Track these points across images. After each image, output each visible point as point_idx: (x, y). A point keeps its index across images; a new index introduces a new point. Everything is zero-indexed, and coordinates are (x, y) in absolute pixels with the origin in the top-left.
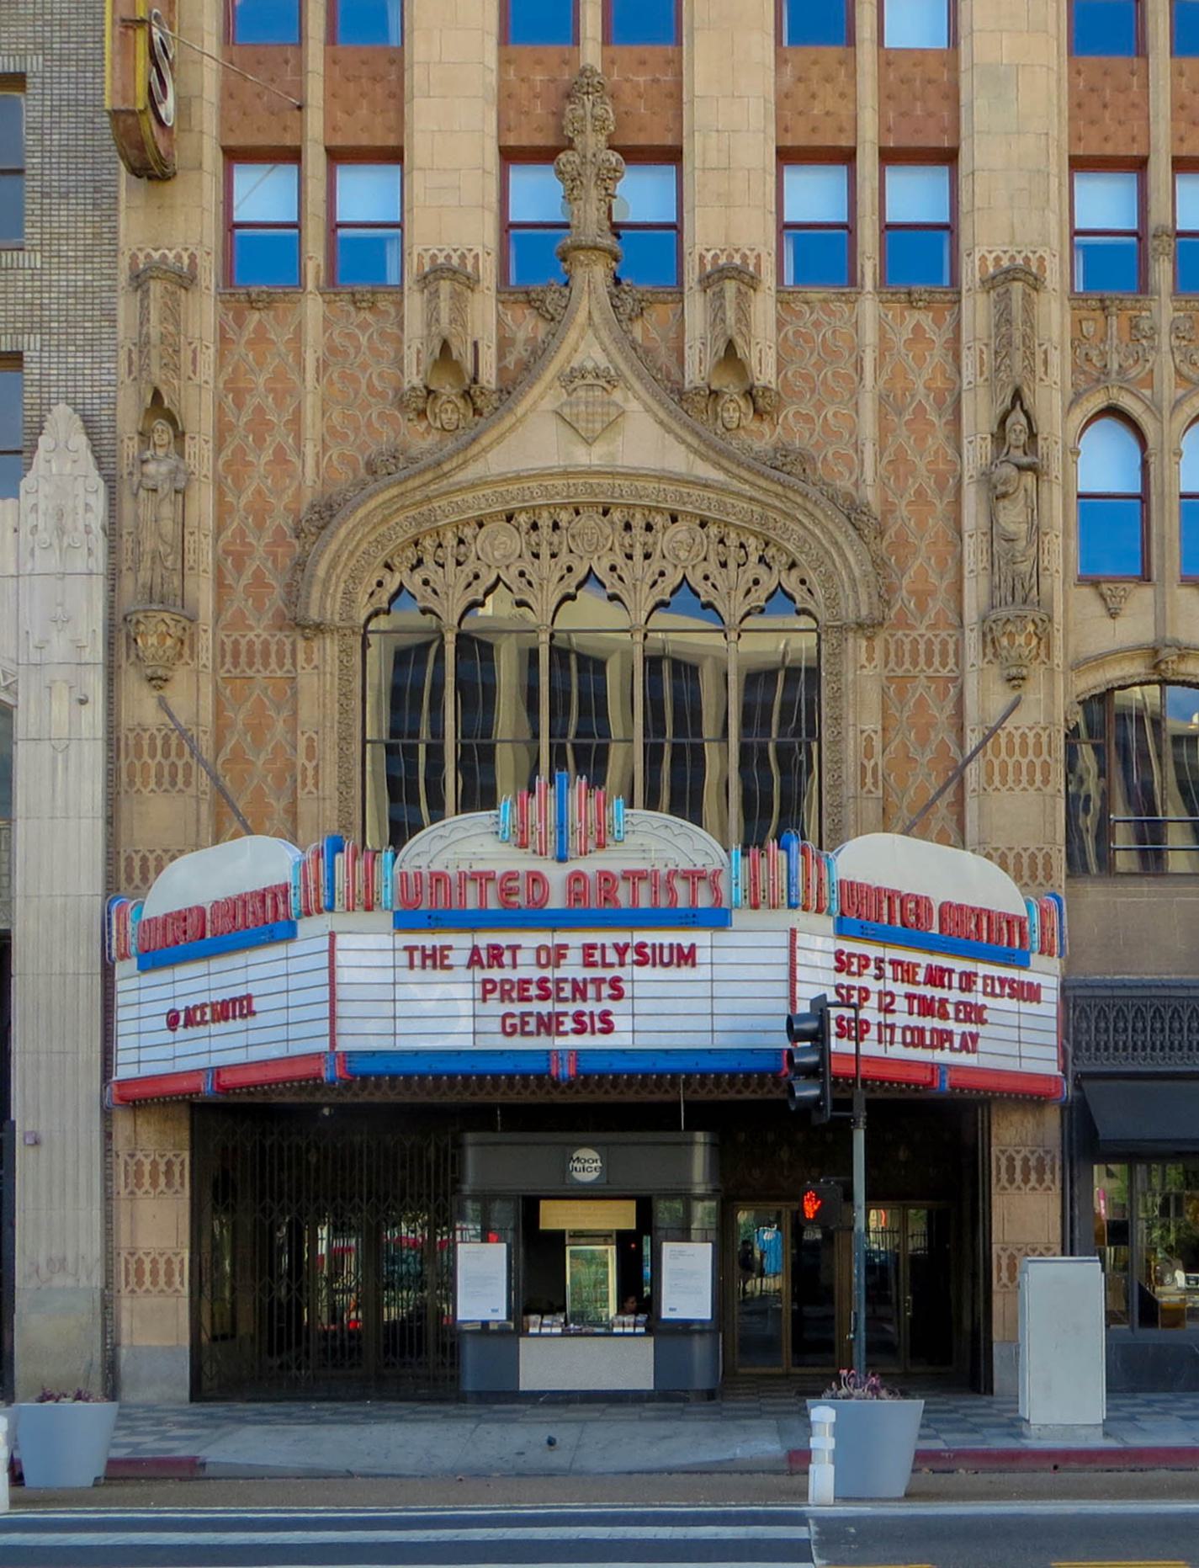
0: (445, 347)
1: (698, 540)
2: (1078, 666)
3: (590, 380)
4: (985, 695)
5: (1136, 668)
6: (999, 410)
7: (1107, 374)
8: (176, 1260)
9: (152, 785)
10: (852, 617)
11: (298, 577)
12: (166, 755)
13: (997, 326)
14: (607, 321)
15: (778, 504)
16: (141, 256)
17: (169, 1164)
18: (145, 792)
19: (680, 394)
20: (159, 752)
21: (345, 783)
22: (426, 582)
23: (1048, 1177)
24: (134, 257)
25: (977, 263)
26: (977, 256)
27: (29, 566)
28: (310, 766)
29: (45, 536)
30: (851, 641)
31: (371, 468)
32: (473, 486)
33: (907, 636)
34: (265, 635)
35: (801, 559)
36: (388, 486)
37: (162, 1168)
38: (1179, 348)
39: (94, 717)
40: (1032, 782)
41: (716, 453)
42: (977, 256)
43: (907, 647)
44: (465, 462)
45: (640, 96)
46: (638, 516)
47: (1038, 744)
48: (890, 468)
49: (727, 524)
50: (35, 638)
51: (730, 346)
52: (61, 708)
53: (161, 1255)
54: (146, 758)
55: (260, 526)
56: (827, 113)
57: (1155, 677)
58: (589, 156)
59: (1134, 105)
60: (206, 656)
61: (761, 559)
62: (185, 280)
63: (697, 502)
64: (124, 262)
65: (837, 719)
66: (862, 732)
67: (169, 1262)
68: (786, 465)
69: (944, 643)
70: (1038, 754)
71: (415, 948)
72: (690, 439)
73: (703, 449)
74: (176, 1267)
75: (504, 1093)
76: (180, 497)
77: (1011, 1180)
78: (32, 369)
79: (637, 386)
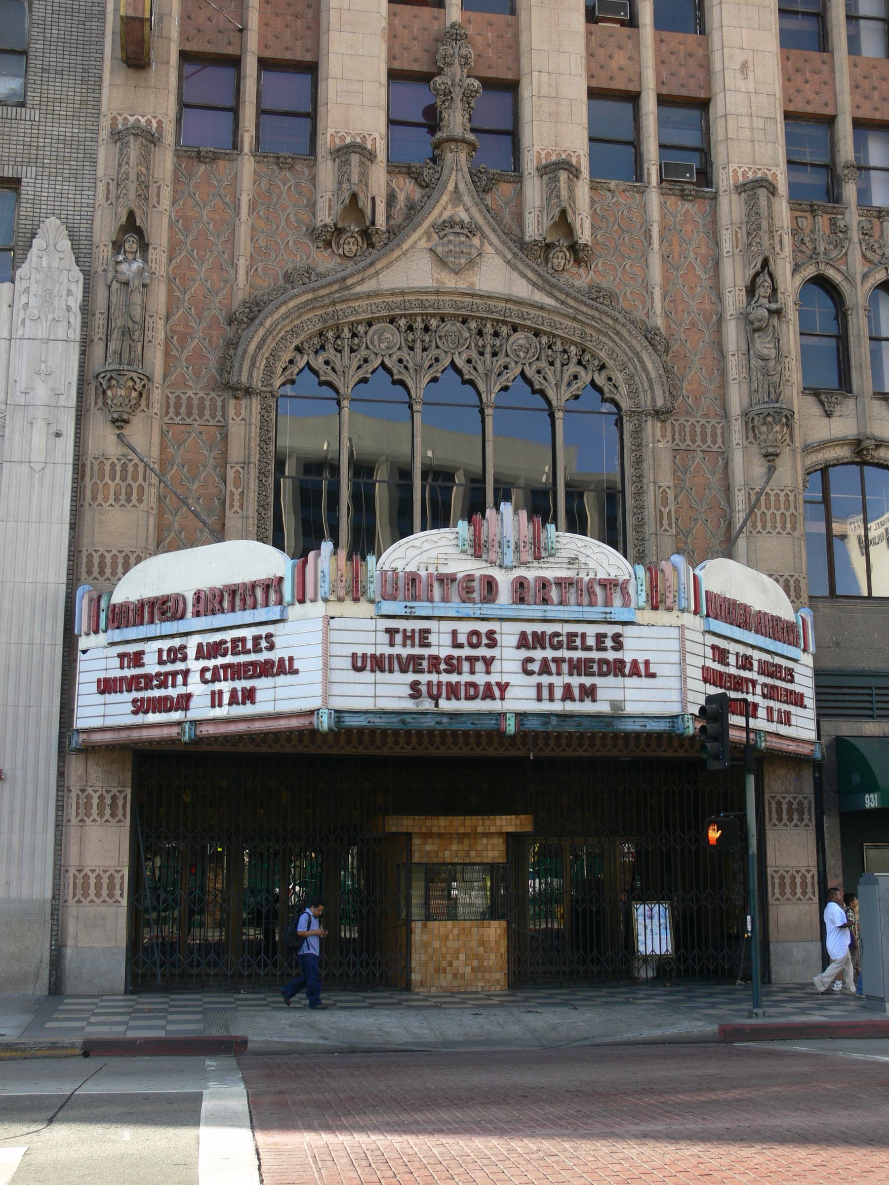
0: (354, 197)
1: (533, 345)
2: (808, 449)
3: (457, 229)
4: (746, 466)
5: (844, 453)
6: (752, 272)
7: (817, 254)
8: (118, 876)
9: (111, 501)
10: (649, 407)
11: (231, 352)
12: (124, 479)
13: (748, 215)
14: (470, 191)
15: (594, 323)
16: (120, 119)
17: (114, 798)
18: (105, 505)
19: (522, 245)
20: (118, 476)
21: (262, 506)
22: (327, 363)
23: (806, 816)
24: (114, 119)
25: (731, 174)
26: (731, 169)
27: (20, 333)
28: (237, 493)
29: (35, 311)
30: (649, 422)
31: (288, 277)
32: (368, 296)
33: (687, 421)
34: (201, 394)
35: (610, 363)
36: (304, 293)
37: (108, 801)
38: (864, 240)
39: (67, 444)
40: (784, 528)
41: (548, 287)
42: (731, 169)
43: (688, 429)
44: (363, 279)
45: (488, 45)
46: (489, 325)
47: (787, 500)
48: (672, 305)
49: (554, 336)
50: (22, 385)
51: (563, 213)
52: (39, 438)
53: (105, 872)
54: (107, 479)
55: (200, 316)
56: (621, 69)
57: (858, 460)
58: (457, 81)
59: (825, 83)
60: (156, 407)
61: (579, 363)
62: (151, 139)
63: (534, 318)
64: (105, 123)
66: (660, 487)
67: (111, 877)
68: (598, 295)
69: (714, 428)
70: (788, 509)
71: (397, 631)
72: (530, 275)
73: (540, 282)
74: (117, 882)
75: (391, 748)
77: (780, 819)
78: (27, 190)
79: (492, 236)
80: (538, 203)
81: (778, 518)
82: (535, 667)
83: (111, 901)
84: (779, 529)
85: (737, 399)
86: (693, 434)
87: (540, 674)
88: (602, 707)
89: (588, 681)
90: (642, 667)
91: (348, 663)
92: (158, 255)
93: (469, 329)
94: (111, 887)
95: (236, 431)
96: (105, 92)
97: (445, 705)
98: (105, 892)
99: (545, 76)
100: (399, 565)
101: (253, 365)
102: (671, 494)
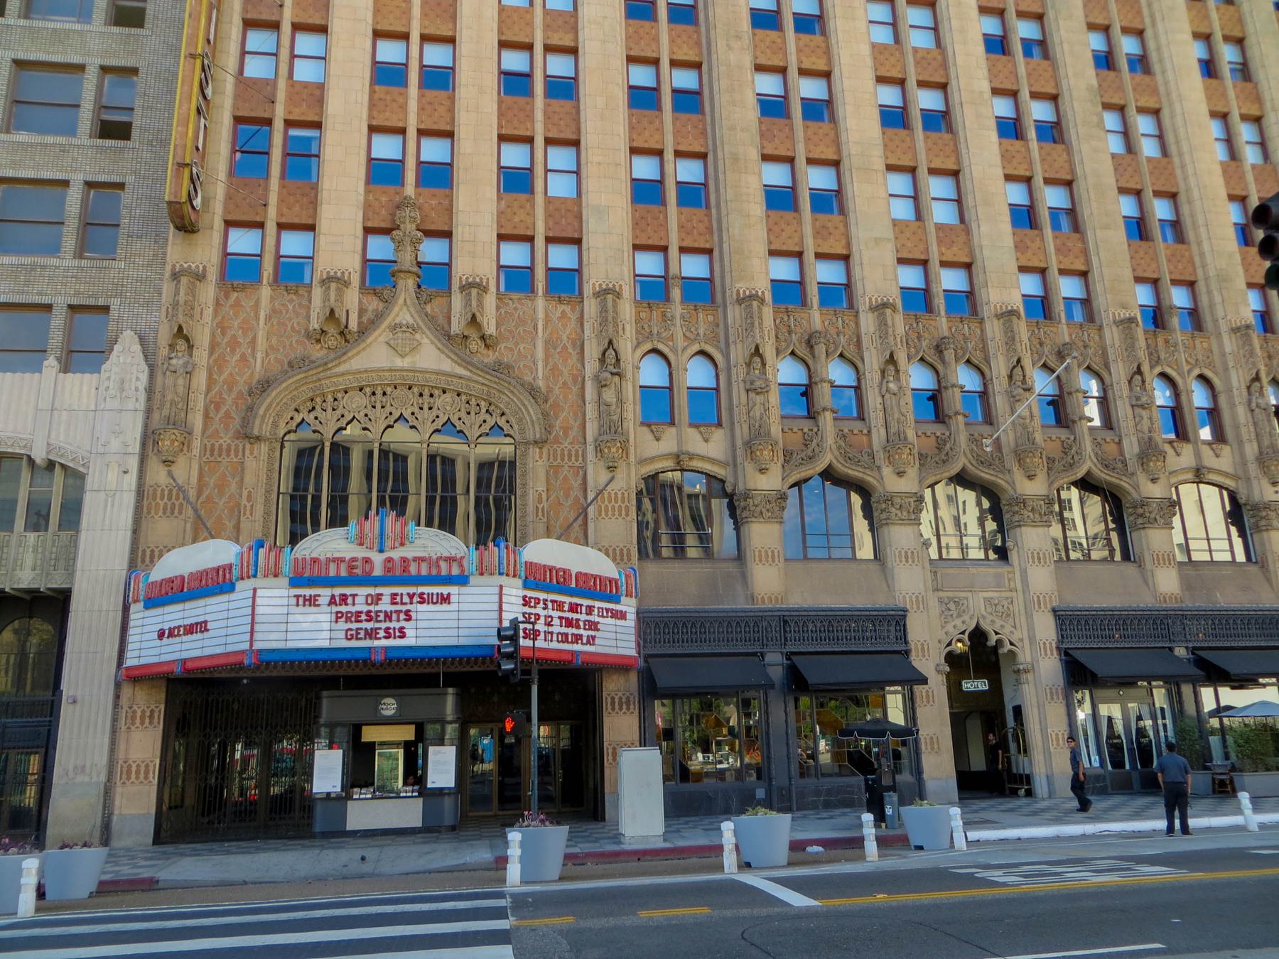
0: (332, 311)
2: (642, 462)
4: (597, 475)
5: (669, 464)
6: (602, 349)
8: (151, 765)
12: (170, 499)
17: (152, 712)
21: (267, 513)
24: (174, 266)
31: (291, 365)
32: (343, 374)
35: (507, 411)
37: (148, 714)
39: (131, 481)
41: (467, 364)
47: (623, 497)
52: (113, 475)
55: (230, 390)
62: (200, 277)
63: (456, 384)
64: (168, 268)
67: (147, 766)
69: (577, 451)
74: (151, 769)
77: (613, 709)
78: (114, 314)
80: (872, 330)
85: (591, 430)
92: (201, 355)
94: (147, 773)
95: (250, 464)
96: (169, 248)
98: (142, 776)
100: (307, 553)
101: (263, 422)
102: (544, 496)
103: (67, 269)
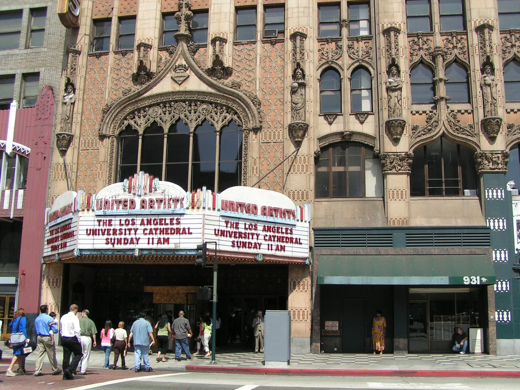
17: (57, 280)
37: (55, 281)
42: (288, 29)
43: (268, 134)
54: (59, 171)
65: (246, 155)
76: (72, 106)
78: (41, 75)
81: (300, 167)
82: (148, 232)
83: (299, 321)
84: (300, 171)
86: (270, 135)
87: (149, 234)
88: (171, 246)
89: (166, 236)
90: (187, 231)
91: (85, 232)
93: (186, 104)
97: (117, 247)
99: (216, 5)
103: (22, 55)
